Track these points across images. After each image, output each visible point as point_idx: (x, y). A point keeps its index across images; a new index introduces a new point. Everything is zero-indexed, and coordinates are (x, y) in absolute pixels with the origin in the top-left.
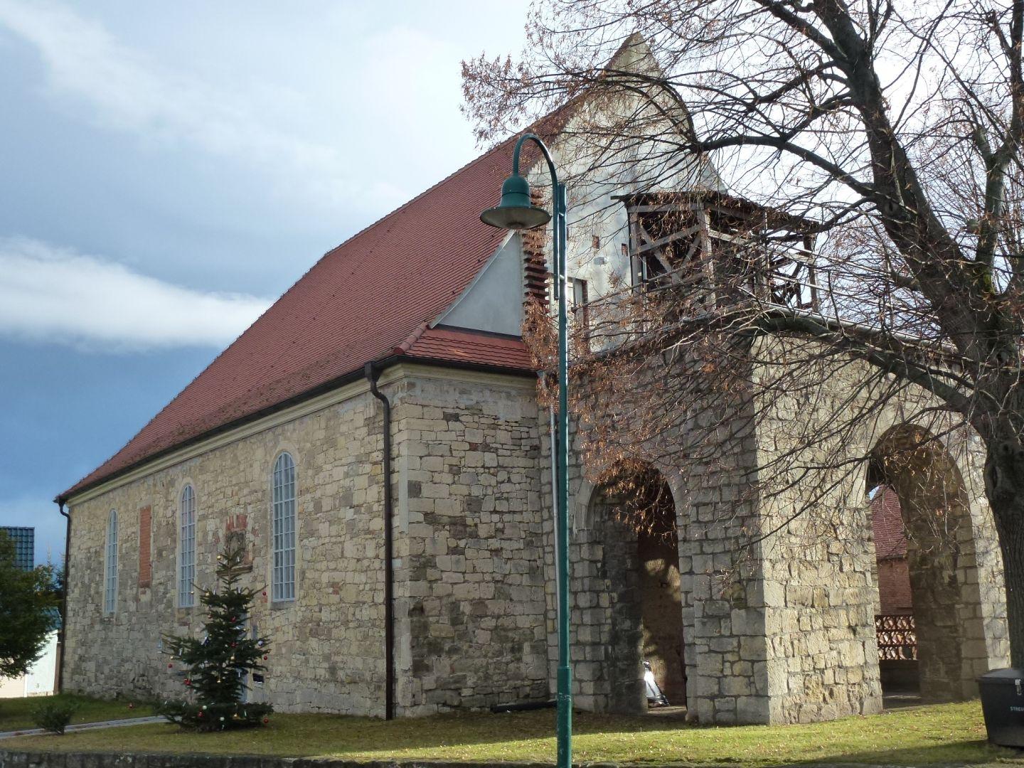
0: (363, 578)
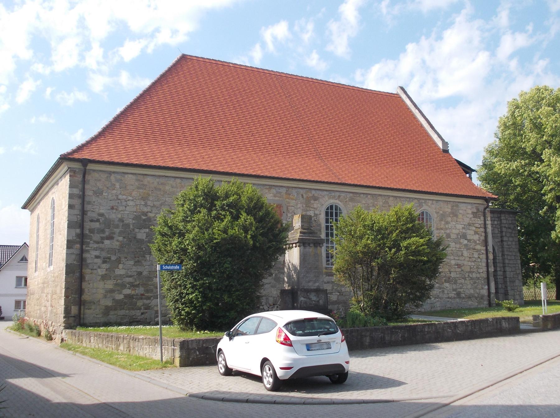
0: (473, 264)
